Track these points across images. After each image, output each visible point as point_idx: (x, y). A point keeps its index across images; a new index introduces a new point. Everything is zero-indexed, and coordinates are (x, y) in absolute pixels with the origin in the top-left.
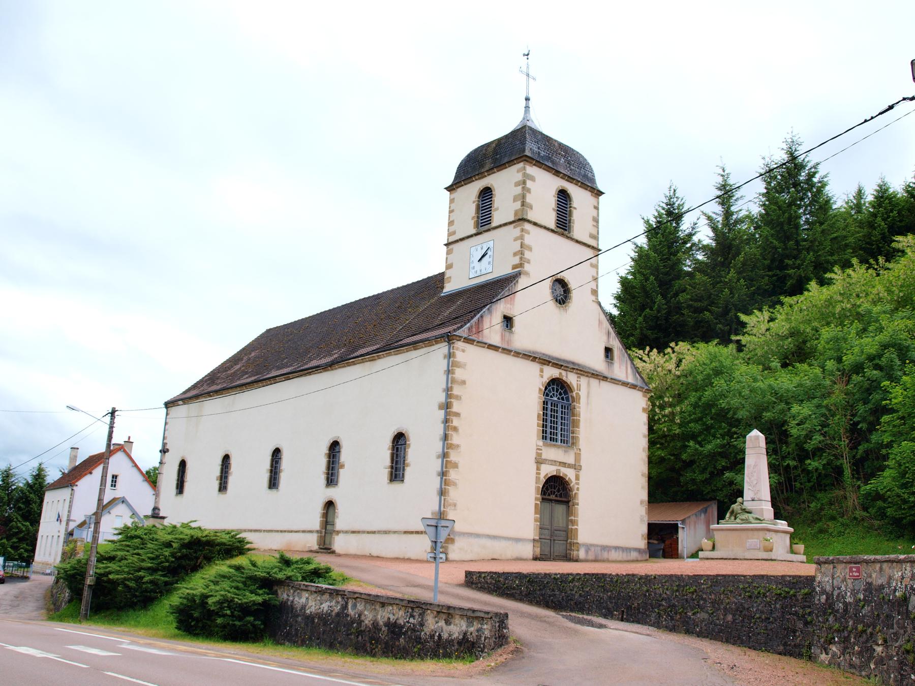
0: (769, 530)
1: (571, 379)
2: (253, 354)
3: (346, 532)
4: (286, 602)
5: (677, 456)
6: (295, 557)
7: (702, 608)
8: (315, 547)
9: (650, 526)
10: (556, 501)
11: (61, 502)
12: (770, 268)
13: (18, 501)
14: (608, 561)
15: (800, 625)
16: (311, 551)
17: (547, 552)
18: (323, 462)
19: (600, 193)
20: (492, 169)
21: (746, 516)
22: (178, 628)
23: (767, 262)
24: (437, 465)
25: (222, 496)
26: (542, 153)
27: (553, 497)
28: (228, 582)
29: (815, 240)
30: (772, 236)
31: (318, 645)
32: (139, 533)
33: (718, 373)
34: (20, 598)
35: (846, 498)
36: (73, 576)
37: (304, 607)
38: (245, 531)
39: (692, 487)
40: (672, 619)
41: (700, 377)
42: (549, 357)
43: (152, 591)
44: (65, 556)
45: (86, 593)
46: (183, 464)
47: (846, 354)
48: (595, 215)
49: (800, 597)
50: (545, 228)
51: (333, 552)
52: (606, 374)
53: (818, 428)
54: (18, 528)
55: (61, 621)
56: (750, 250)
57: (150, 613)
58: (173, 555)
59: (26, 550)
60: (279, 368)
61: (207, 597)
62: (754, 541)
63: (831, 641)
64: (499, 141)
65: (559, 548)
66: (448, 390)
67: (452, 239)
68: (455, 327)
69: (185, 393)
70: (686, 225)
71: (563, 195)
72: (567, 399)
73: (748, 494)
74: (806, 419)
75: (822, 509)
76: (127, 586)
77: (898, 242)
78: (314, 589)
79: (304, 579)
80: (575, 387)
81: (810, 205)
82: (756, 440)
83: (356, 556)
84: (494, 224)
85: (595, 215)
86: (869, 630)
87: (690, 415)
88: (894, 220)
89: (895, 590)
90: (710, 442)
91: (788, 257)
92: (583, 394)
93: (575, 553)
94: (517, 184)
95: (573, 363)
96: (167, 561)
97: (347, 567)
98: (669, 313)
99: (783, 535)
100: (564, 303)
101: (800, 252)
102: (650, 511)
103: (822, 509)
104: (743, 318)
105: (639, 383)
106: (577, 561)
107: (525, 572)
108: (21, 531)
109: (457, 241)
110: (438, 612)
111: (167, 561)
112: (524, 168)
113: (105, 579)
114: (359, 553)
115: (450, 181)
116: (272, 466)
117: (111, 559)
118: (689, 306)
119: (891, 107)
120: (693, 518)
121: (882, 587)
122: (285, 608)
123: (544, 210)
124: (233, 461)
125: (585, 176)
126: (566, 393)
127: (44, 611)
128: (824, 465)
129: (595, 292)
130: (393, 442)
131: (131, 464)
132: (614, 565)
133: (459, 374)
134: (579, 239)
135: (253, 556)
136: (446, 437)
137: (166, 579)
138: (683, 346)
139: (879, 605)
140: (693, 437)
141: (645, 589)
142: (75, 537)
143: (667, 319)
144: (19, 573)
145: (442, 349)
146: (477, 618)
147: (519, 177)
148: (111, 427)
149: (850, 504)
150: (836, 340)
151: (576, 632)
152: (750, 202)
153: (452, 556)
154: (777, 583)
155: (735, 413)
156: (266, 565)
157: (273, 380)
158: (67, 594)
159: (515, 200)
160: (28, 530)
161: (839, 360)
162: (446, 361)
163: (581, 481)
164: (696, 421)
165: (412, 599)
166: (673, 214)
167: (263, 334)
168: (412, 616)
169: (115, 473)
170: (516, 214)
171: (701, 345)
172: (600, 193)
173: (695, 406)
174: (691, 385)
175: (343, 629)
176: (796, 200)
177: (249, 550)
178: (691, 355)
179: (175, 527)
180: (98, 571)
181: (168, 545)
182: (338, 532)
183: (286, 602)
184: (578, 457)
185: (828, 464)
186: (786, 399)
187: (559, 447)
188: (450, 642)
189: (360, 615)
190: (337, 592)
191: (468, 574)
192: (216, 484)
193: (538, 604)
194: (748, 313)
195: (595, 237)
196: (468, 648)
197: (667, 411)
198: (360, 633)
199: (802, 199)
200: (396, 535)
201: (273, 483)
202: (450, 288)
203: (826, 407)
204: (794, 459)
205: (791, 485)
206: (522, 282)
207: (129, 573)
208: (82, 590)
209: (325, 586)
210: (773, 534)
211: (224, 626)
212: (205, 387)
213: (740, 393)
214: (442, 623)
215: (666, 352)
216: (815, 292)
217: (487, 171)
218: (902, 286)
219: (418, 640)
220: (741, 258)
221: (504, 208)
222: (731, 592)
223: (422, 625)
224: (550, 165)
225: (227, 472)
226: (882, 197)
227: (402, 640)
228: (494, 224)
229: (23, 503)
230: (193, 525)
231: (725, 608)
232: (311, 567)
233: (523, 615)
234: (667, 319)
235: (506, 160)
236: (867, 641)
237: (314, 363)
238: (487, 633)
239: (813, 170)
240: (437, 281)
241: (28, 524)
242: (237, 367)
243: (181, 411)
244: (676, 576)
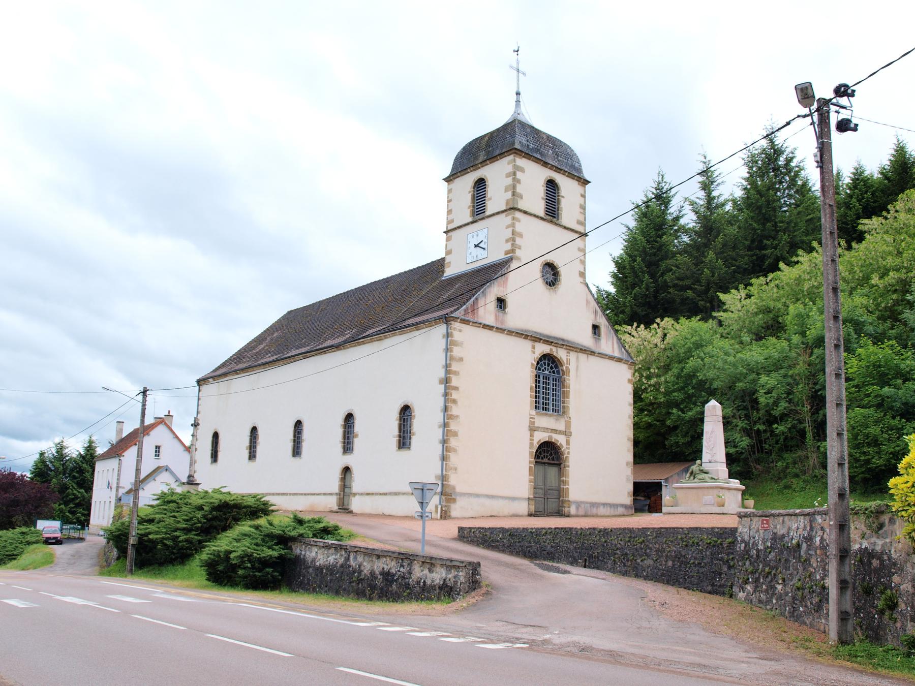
0: (722, 488)
1: (561, 354)
2: (276, 335)
3: (362, 494)
4: (299, 556)
5: (663, 422)
6: (307, 517)
7: (648, 556)
8: (335, 508)
9: (636, 485)
10: (549, 464)
11: (111, 470)
12: (750, 248)
13: (72, 470)
14: (597, 516)
15: (725, 568)
16: (331, 511)
17: (541, 509)
18: (340, 432)
19: (586, 182)
20: (485, 161)
21: (704, 475)
22: (208, 580)
23: (747, 243)
24: (439, 434)
25: (252, 464)
26: (531, 146)
27: (546, 460)
28: (249, 540)
29: (791, 221)
30: (752, 218)
31: (326, 592)
32: (174, 498)
33: (698, 346)
34: (77, 556)
35: (808, 458)
36: (118, 537)
37: (314, 560)
38: (270, 494)
39: (675, 449)
40: (625, 565)
41: (682, 351)
42: (541, 334)
43: (187, 548)
44: (118, 517)
45: (130, 551)
46: (216, 436)
47: (810, 329)
48: (582, 203)
49: (725, 546)
50: (535, 216)
51: (351, 512)
52: (594, 348)
53: (783, 396)
54: (74, 494)
55: (110, 576)
56: (733, 230)
57: (187, 567)
58: (204, 517)
59: (83, 515)
60: (298, 348)
61: (230, 552)
62: (709, 497)
63: (746, 582)
64: (492, 133)
65: (552, 505)
66: (447, 366)
67: (451, 227)
68: (452, 309)
69: (215, 371)
70: (673, 209)
71: (551, 185)
72: (558, 372)
73: (706, 456)
74: (773, 388)
75: (787, 467)
76: (165, 545)
77: (864, 224)
78: (321, 544)
79: (315, 536)
81: (787, 188)
82: (714, 410)
83: (370, 516)
84: (488, 213)
85: (582, 203)
86: (774, 572)
87: (673, 385)
88: (868, 201)
89: (792, 539)
90: (691, 409)
91: (768, 238)
92: (572, 367)
93: (567, 509)
94: (508, 175)
95: (563, 340)
96: (200, 522)
97: (358, 525)
98: (657, 291)
99: (735, 492)
100: (554, 285)
101: (777, 232)
102: (635, 472)
103: (787, 467)
104: (722, 296)
105: (625, 356)
106: (568, 516)
107: (507, 527)
108: (77, 498)
109: (455, 229)
110: (423, 562)
111: (200, 522)
112: (514, 161)
113: (146, 538)
114: (373, 512)
115: (447, 173)
116: (295, 436)
117: (151, 521)
118: (675, 286)
119: (788, 124)
120: (676, 477)
121: (783, 536)
122: (298, 561)
123: (535, 201)
124: (260, 433)
125: (572, 166)
126: (556, 367)
127: (97, 568)
128: (790, 429)
129: (582, 275)
130: (400, 414)
131: (172, 436)
132: (605, 520)
133: (456, 352)
134: (567, 226)
135: (276, 519)
136: (446, 409)
137: (200, 538)
138: (667, 322)
139: (781, 551)
140: (677, 405)
141: (603, 540)
142: (122, 502)
143: (655, 297)
144: (76, 535)
145: (441, 329)
146: (454, 566)
147: (510, 168)
148: (144, 405)
149: (811, 463)
150: (799, 315)
151: (542, 577)
152: (732, 185)
153: (454, 513)
154: (708, 534)
155: (711, 384)
156: (282, 524)
157: (293, 359)
158: (115, 552)
159: (506, 191)
160: (83, 496)
161: (803, 334)
162: (445, 340)
163: (571, 446)
164: (679, 390)
165: (402, 551)
166: (662, 197)
167: (285, 315)
168: (402, 566)
169: (158, 444)
170: (507, 203)
171: (683, 320)
172: (586, 182)
173: (678, 377)
174: (672, 359)
175: (346, 578)
176: (775, 183)
177: (273, 511)
178: (675, 330)
179: (207, 492)
180: (139, 532)
181: (200, 508)
182: (355, 494)
183: (299, 556)
184: (568, 424)
185: (794, 427)
186: (756, 370)
187: (550, 416)
188: (433, 587)
189: (360, 566)
190: (341, 547)
191: (461, 529)
192: (246, 453)
193: (511, 553)
194: (726, 291)
195: (583, 223)
196: (447, 591)
197: (653, 381)
198: (360, 581)
199: (781, 183)
200: (405, 496)
201: (297, 451)
202: (449, 272)
203: (792, 376)
204: (764, 424)
205: (762, 447)
206: (514, 265)
207: (166, 533)
208: (126, 548)
209: (330, 542)
210: (726, 491)
211: (245, 577)
212: (233, 365)
213: (714, 366)
214: (426, 571)
215: (652, 327)
216: (786, 273)
217: (481, 163)
218: (862, 266)
219: (407, 586)
220: (720, 239)
221: (496, 199)
222: (672, 542)
223: (410, 573)
224: (539, 156)
225: (255, 443)
226: (858, 179)
227: (394, 586)
228: (488, 213)
229: (77, 472)
230: (224, 490)
231: (667, 556)
232: (321, 525)
233: (500, 563)
234: (655, 297)
235: (498, 152)
236: (771, 581)
237: (329, 343)
238: (462, 579)
239: (791, 155)
240: (438, 266)
241: (83, 491)
242: (261, 347)
243: (211, 389)
244: (629, 529)
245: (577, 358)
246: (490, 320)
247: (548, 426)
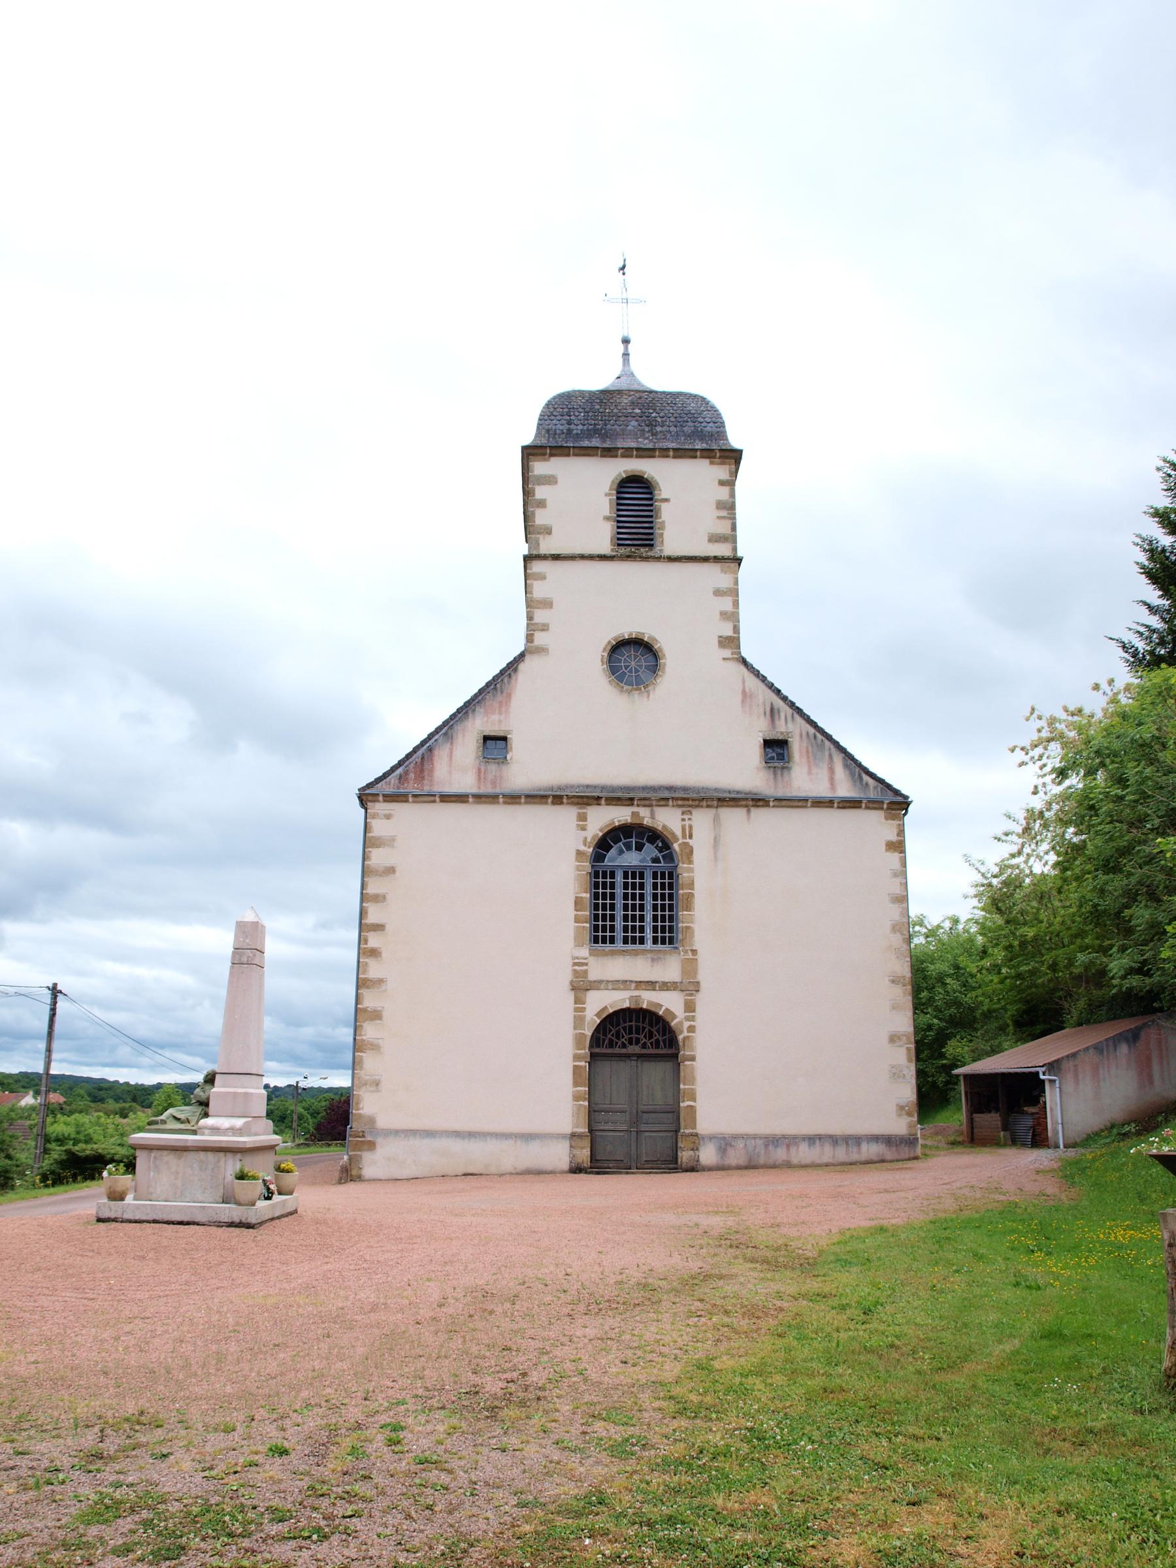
1: (668, 819)
10: (640, 1056)
80: (679, 833)
106: (692, 1169)
153: (368, 1171)
184: (690, 966)
195: (731, 538)
247: (629, 976)
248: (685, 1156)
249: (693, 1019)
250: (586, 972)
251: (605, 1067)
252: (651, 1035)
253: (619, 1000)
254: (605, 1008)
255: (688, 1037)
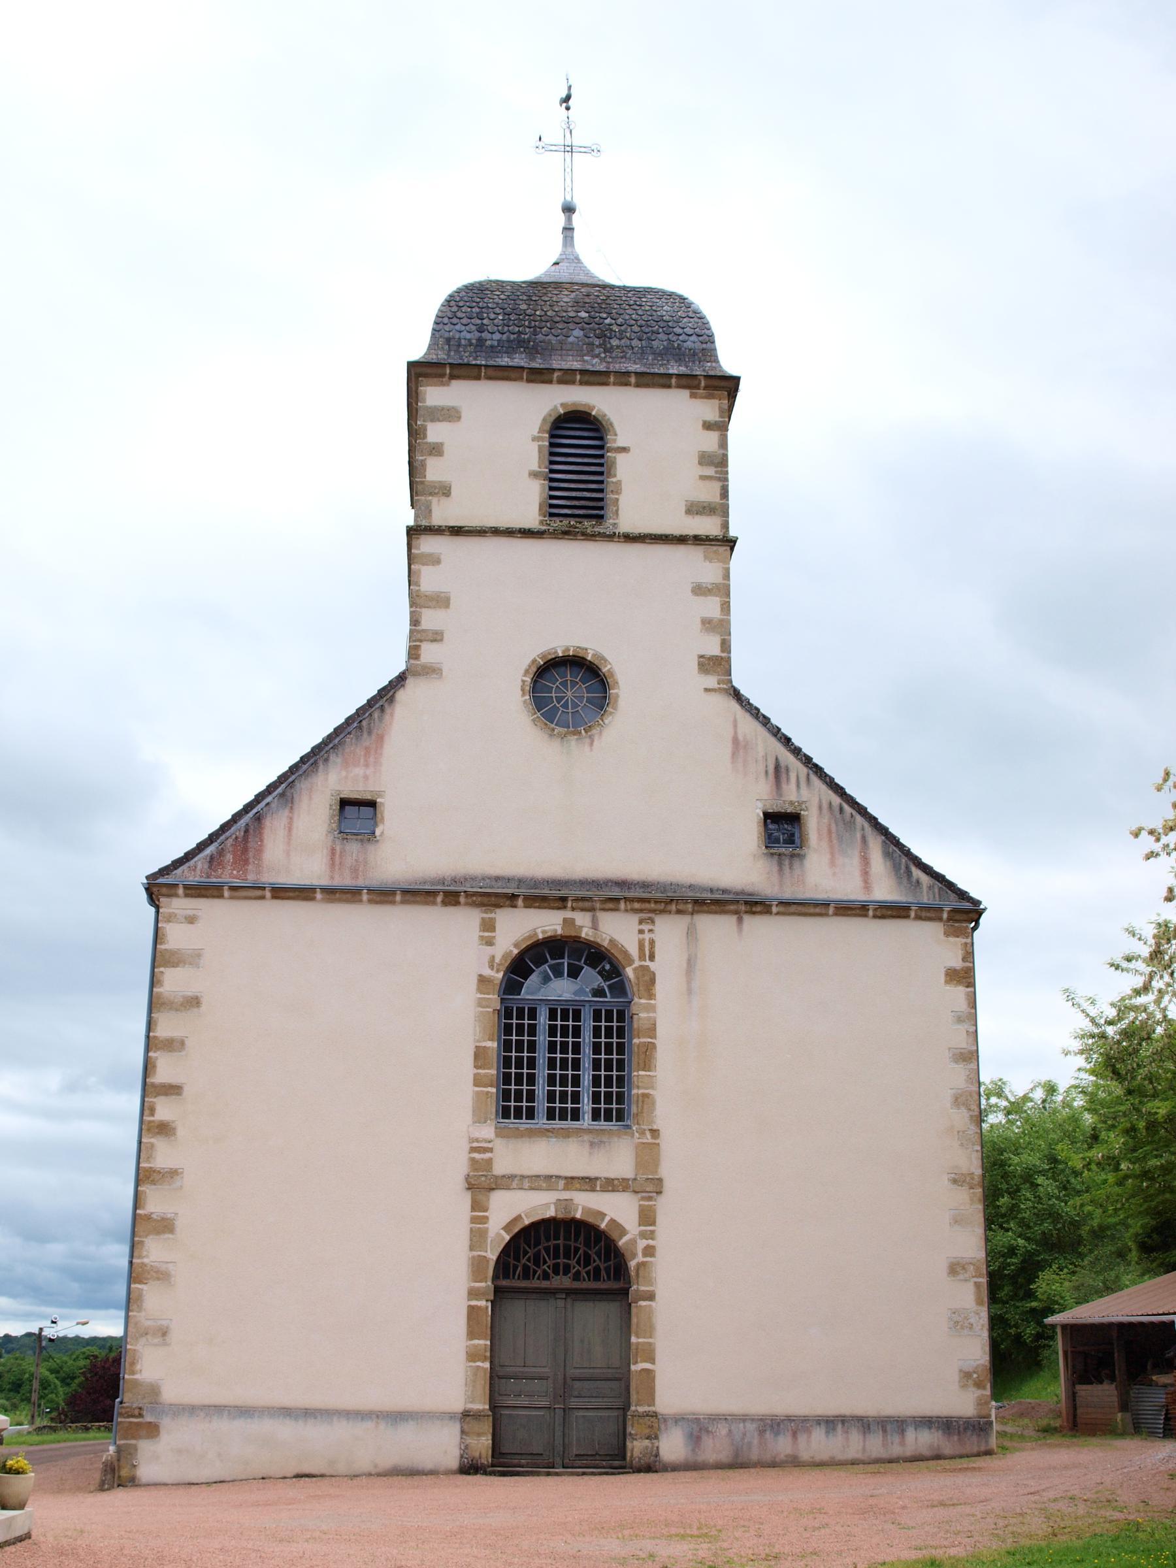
1: (617, 930)
10: (569, 1293)
106: (648, 1469)
153: (145, 1472)
184: (649, 1155)
195: (721, 509)
245: (691, 933)
246: (310, 868)
247: (552, 1168)
248: (637, 1447)
249: (651, 1235)
250: (489, 1162)
251: (517, 1310)
252: (587, 1260)
253: (538, 1205)
254: (518, 1218)
255: (644, 1264)
